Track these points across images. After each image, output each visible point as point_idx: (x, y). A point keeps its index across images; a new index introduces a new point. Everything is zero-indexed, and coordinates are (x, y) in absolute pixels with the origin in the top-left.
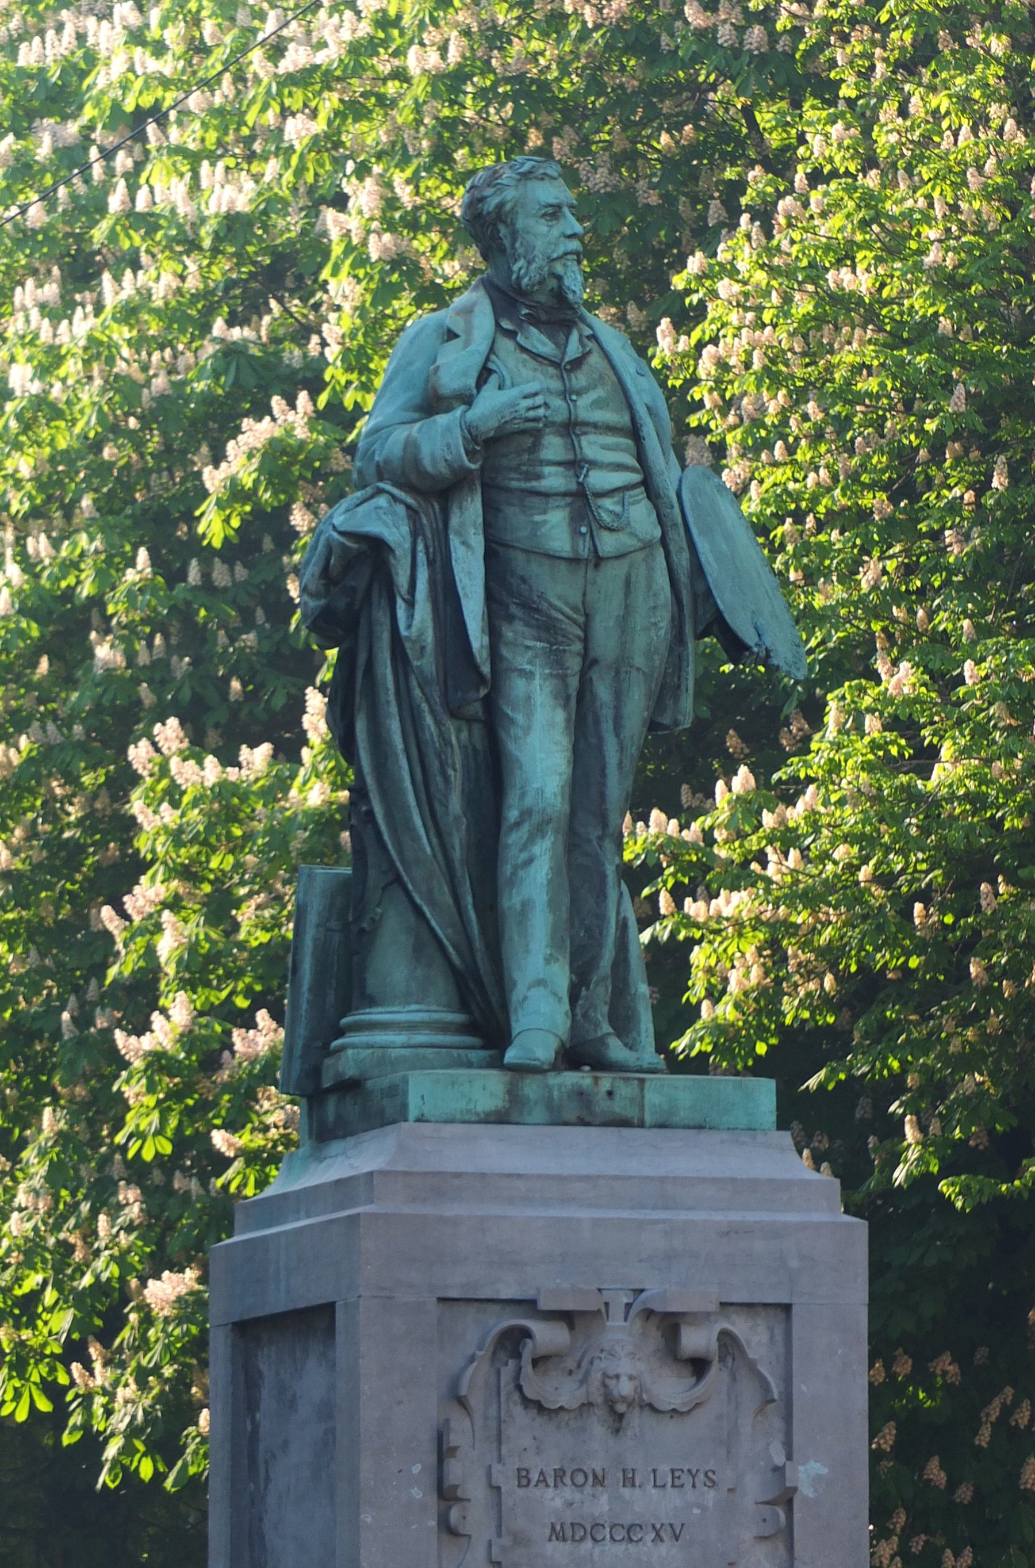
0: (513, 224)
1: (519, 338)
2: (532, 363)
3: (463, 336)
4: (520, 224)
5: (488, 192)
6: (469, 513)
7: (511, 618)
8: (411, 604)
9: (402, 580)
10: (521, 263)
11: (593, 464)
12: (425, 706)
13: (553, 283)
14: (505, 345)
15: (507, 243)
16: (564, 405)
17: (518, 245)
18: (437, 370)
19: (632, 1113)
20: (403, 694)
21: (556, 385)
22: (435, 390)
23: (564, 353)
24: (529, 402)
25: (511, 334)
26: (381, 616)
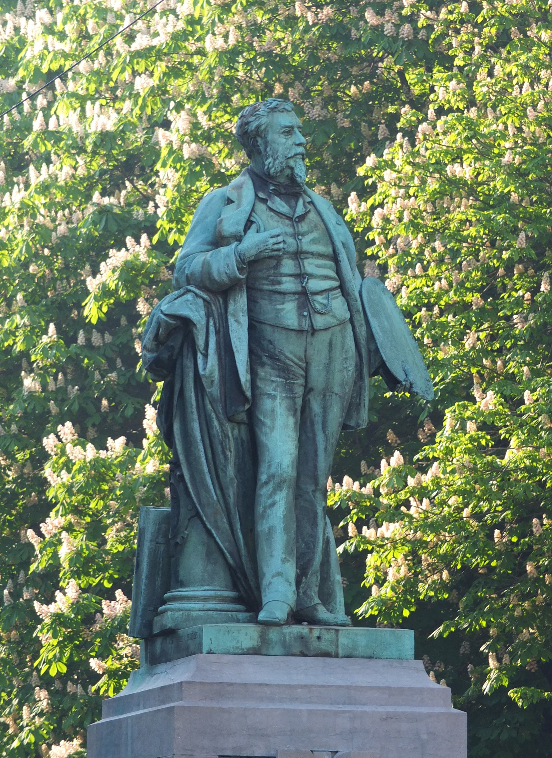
2: (276, 218)
3: (236, 202)
4: (269, 138)
6: (239, 304)
7: (263, 365)
8: (206, 356)
9: (200, 342)
11: (311, 276)
13: (288, 172)
14: (261, 207)
15: (262, 148)
17: (268, 149)
19: (331, 649)
20: (201, 408)
21: (290, 230)
22: (220, 232)
23: (294, 212)
25: (264, 201)
26: (189, 363)
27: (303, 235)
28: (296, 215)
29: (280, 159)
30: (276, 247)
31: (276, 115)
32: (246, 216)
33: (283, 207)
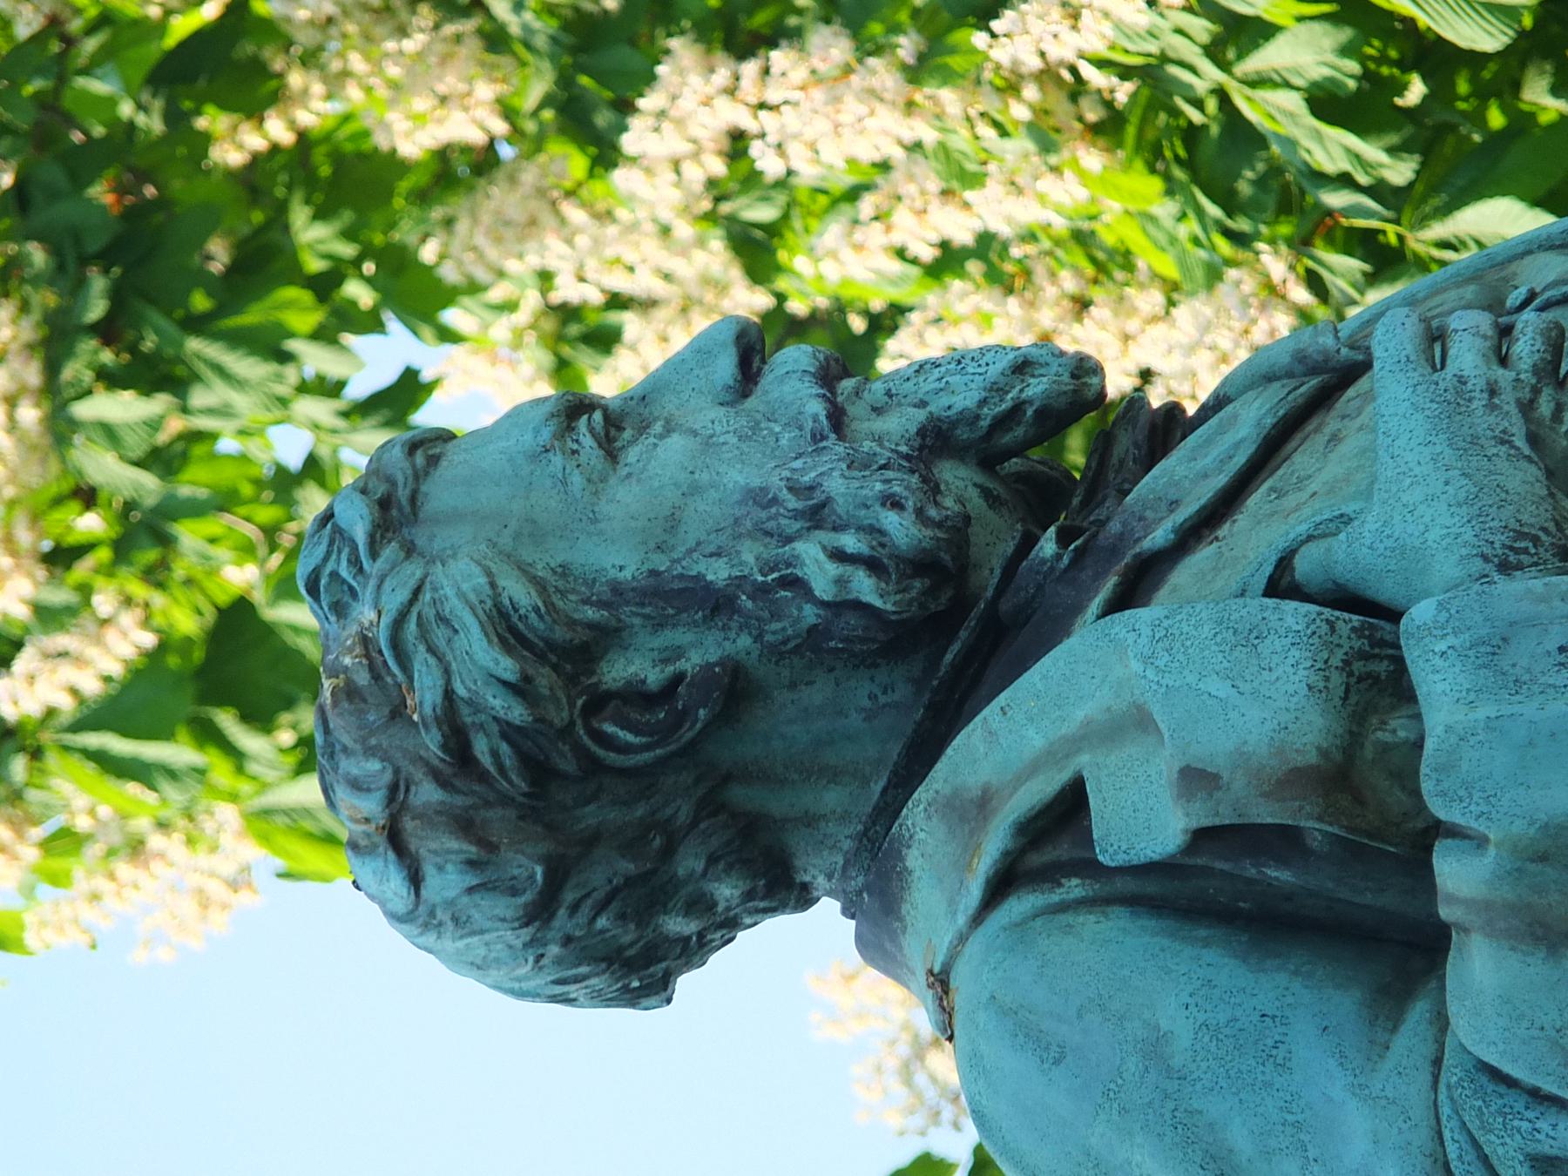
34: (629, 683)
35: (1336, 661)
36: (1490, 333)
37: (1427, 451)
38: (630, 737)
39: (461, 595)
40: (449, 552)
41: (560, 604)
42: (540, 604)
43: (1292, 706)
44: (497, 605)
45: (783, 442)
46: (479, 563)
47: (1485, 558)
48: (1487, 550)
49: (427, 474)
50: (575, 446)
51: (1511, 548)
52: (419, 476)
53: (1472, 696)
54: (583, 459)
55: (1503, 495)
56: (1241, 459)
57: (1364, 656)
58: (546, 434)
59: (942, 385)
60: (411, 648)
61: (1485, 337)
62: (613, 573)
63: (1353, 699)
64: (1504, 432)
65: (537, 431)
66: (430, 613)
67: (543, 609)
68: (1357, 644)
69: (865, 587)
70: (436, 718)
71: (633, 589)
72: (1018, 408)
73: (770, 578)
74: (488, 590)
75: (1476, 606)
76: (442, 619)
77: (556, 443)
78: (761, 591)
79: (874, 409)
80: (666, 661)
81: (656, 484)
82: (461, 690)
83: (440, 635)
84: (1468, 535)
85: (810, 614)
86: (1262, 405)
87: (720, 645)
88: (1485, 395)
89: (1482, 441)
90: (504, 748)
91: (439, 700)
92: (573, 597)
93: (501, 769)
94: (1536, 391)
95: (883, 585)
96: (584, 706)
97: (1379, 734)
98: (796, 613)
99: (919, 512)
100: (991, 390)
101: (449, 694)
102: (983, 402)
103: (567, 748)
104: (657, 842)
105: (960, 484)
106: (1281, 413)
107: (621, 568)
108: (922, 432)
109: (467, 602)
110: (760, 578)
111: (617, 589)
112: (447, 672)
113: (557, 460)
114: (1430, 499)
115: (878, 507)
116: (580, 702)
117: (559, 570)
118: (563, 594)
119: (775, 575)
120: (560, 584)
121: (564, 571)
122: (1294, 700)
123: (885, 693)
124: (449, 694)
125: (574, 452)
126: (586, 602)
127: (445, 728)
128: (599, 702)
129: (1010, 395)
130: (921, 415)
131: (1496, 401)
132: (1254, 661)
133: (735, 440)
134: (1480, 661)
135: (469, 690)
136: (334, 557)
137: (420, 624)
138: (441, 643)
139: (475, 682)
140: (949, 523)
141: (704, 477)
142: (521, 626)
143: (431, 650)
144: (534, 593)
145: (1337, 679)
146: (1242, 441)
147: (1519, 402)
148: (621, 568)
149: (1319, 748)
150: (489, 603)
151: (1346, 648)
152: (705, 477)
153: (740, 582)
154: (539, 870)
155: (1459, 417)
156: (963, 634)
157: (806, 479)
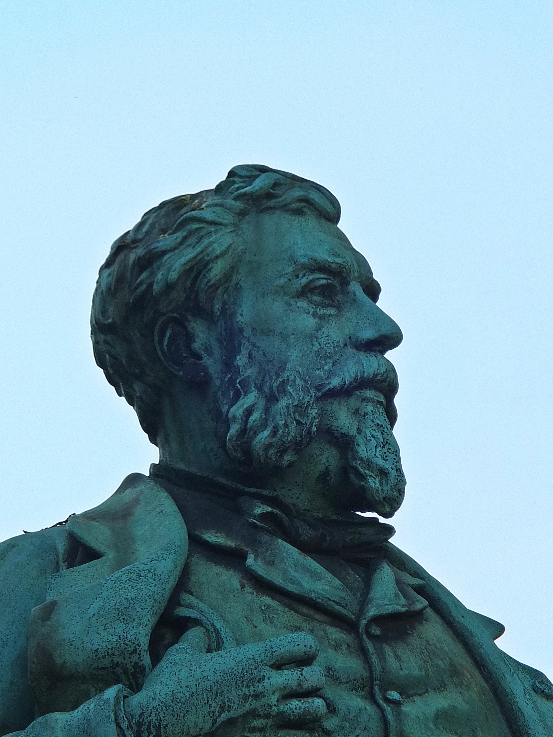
0: (228, 314)
1: (250, 561)
2: (286, 615)
3: (110, 555)
4: (245, 313)
5: (166, 241)
10: (250, 398)
12: (178, 222)
13: (327, 457)
14: (215, 578)
15: (212, 364)
16: (370, 708)
17: (241, 360)
18: (49, 610)
21: (347, 663)
22: (46, 655)
23: (364, 600)
24: (288, 677)
25: (232, 558)
27: (410, 689)
28: (372, 612)
29: (295, 394)
30: (295, 706)
31: (269, 222)
32: (162, 590)
33: (315, 576)
34: (194, 335)
35: (115, 660)
36: (305, 687)
37: (211, 673)
38: (165, 343)
39: (210, 244)
40: (240, 233)
41: (220, 291)
42: (212, 282)
43: (85, 645)
44: (208, 263)
45: (318, 372)
46: (228, 248)
47: (141, 716)
48: (146, 715)
49: (287, 211)
50: (300, 276)
51: (149, 726)
52: (285, 208)
53: (67, 727)
54: (295, 281)
55: (182, 715)
56: (290, 587)
57: (125, 671)
58: (302, 260)
59: (369, 438)
60: (184, 229)
61: (299, 685)
62: (239, 311)
63: (103, 673)
64: (229, 707)
65: (305, 256)
66: (203, 232)
67: (209, 284)
68: (129, 666)
69: (234, 429)
70: (150, 251)
71: (232, 323)
72: (362, 477)
73: (238, 385)
74: (214, 256)
75: (103, 717)
76: (200, 239)
77: (299, 266)
78: (232, 381)
79: (357, 410)
80: (206, 349)
81: (284, 319)
82: (165, 258)
83: (192, 240)
84: (153, 704)
85: (225, 409)
86: (326, 591)
87: (215, 372)
88: (252, 693)
89: (219, 698)
90: (145, 286)
91: (159, 249)
92: (226, 297)
93: (136, 288)
94: (267, 716)
95: (234, 439)
96: (174, 317)
97: (93, 689)
98: (225, 402)
99: (270, 445)
100: (369, 462)
101: (164, 253)
102: (362, 459)
103: (152, 316)
104: (137, 371)
105: (324, 460)
106: (319, 600)
107: (242, 315)
108: (344, 435)
109: (207, 248)
110: (238, 381)
111: (233, 315)
112: (174, 249)
113: (290, 269)
114: (179, 682)
115: (273, 425)
116: (175, 315)
117: (239, 286)
118: (226, 291)
119: (239, 387)
120: (231, 289)
121: (238, 288)
122: (89, 645)
123: (215, 455)
124: (164, 253)
125: (297, 276)
126: (224, 303)
127: (148, 256)
128: (180, 322)
129: (367, 472)
130: (353, 431)
131: (250, 699)
132: (109, 620)
133: (315, 349)
134: (81, 726)
135: (165, 262)
136: (241, 180)
137: (197, 229)
138: (189, 242)
139: (169, 263)
140: (269, 461)
141: (292, 340)
142: (201, 276)
143: (185, 239)
144: (217, 278)
145: (107, 662)
146: (300, 585)
147: (254, 710)
148: (242, 315)
149: (65, 663)
150: (208, 258)
151: (125, 662)
152: (293, 340)
153: (237, 371)
154: (110, 321)
155: (234, 684)
156: (229, 483)
157: (289, 387)
